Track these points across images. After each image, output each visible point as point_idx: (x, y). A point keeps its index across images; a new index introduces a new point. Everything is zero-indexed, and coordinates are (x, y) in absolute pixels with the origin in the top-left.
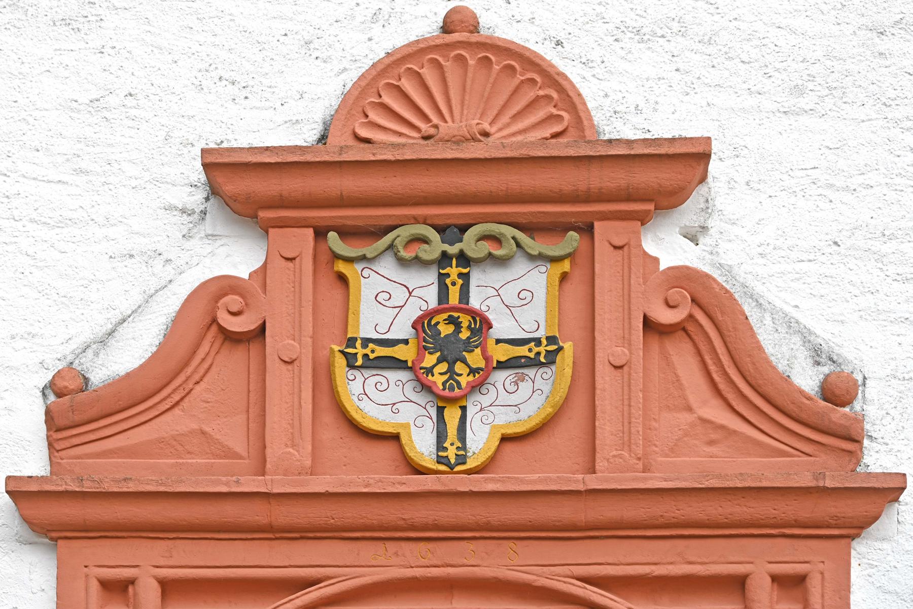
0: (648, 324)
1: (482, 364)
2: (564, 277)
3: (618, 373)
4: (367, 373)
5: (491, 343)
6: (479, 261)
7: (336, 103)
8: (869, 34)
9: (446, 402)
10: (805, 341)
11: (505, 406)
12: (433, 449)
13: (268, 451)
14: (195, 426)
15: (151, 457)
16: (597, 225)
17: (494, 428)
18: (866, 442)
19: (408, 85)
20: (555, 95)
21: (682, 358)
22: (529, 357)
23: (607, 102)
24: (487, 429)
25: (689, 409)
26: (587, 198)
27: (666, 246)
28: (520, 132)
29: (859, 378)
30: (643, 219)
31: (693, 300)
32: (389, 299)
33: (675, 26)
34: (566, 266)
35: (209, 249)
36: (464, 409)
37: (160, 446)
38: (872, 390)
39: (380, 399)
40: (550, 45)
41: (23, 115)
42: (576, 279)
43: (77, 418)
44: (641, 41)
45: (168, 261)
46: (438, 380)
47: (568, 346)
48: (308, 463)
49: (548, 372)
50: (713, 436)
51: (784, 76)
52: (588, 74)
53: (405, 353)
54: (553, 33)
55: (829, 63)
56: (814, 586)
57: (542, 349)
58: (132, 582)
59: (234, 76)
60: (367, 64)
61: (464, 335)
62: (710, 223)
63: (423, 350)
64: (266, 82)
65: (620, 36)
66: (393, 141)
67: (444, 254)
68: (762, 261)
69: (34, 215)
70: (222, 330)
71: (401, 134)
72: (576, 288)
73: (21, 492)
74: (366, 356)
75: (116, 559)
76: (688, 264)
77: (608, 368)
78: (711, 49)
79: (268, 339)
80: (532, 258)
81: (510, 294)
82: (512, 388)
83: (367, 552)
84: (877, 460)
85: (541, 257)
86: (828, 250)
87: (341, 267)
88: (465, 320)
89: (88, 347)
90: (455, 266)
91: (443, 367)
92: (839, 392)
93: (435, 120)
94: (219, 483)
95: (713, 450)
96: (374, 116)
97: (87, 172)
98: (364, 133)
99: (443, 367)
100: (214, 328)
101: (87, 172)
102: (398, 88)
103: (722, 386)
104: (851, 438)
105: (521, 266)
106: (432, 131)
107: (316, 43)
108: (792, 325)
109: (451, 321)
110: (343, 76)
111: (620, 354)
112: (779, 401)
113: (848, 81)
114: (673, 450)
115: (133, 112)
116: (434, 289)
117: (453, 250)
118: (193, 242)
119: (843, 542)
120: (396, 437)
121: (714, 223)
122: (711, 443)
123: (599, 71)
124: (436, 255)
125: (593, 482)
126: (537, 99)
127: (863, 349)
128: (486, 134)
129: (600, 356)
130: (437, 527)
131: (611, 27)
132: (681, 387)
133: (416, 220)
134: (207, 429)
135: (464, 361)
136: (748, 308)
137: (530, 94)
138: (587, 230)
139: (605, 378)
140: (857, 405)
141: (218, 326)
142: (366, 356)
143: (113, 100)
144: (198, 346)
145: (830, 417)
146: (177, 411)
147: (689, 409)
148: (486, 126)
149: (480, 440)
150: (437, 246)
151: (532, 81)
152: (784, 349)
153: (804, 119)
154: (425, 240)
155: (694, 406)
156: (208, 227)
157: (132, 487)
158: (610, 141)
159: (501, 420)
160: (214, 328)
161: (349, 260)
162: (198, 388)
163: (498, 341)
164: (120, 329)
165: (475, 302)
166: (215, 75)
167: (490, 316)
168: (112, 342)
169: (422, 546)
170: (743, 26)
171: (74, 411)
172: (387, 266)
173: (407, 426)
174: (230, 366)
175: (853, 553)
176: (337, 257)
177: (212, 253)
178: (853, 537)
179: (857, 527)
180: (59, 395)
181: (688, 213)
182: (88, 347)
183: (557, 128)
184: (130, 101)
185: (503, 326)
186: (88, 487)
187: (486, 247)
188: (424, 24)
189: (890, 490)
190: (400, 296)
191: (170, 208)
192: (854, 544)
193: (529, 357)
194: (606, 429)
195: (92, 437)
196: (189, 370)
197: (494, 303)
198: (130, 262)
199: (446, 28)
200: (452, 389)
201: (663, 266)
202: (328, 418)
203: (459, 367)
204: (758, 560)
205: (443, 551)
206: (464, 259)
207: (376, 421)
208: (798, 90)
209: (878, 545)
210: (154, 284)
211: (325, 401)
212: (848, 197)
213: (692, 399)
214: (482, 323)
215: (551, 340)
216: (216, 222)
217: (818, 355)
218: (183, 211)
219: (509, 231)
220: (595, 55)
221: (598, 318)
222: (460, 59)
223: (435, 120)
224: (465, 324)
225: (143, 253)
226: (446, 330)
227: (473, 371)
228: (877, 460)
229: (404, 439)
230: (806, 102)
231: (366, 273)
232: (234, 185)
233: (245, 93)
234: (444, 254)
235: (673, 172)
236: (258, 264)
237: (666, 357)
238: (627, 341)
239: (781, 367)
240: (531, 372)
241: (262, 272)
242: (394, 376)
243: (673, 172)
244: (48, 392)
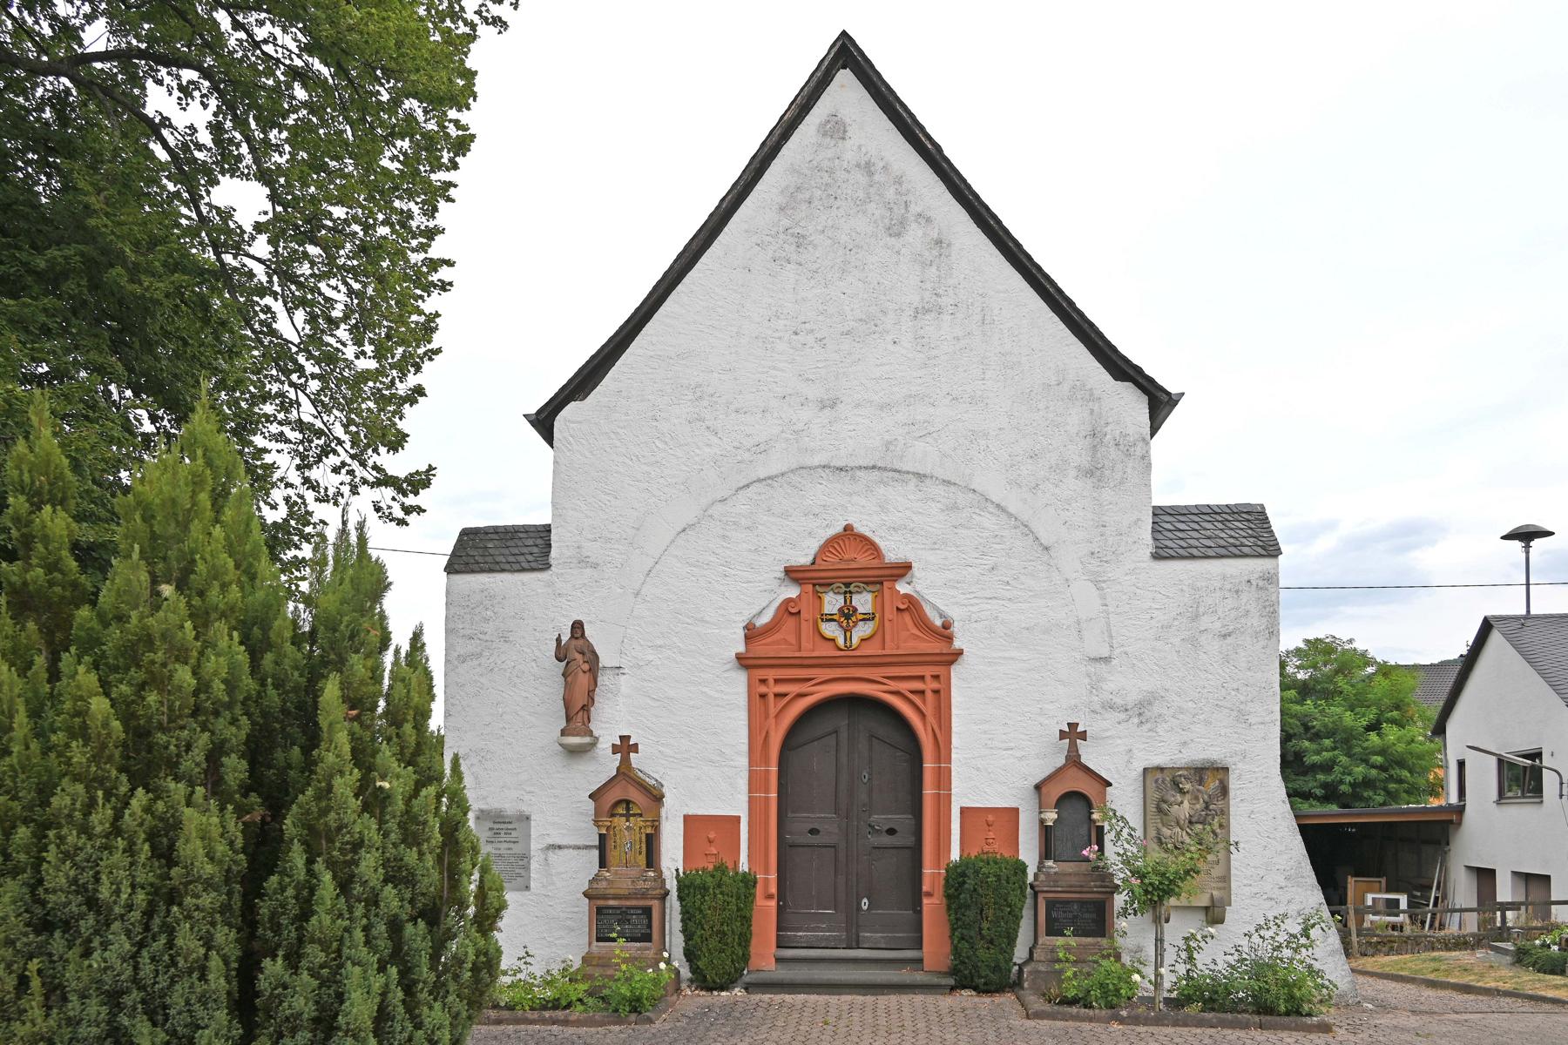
9: (847, 631)
11: (862, 631)
21: (907, 617)
22: (868, 618)
32: (832, 602)
37: (777, 643)
39: (830, 630)
73: (739, 657)
75: (762, 673)
84: (957, 644)
90: (848, 594)
92: (947, 626)
104: (950, 639)
108: (934, 607)
127: (954, 613)
139: (887, 624)
141: (788, 610)
145: (945, 633)
149: (855, 641)
171: (752, 634)
174: (791, 622)
179: (952, 663)
181: (907, 578)
185: (861, 610)
189: (960, 653)
193: (868, 618)
214: (855, 610)
217: (941, 616)
228: (957, 644)
235: (904, 569)
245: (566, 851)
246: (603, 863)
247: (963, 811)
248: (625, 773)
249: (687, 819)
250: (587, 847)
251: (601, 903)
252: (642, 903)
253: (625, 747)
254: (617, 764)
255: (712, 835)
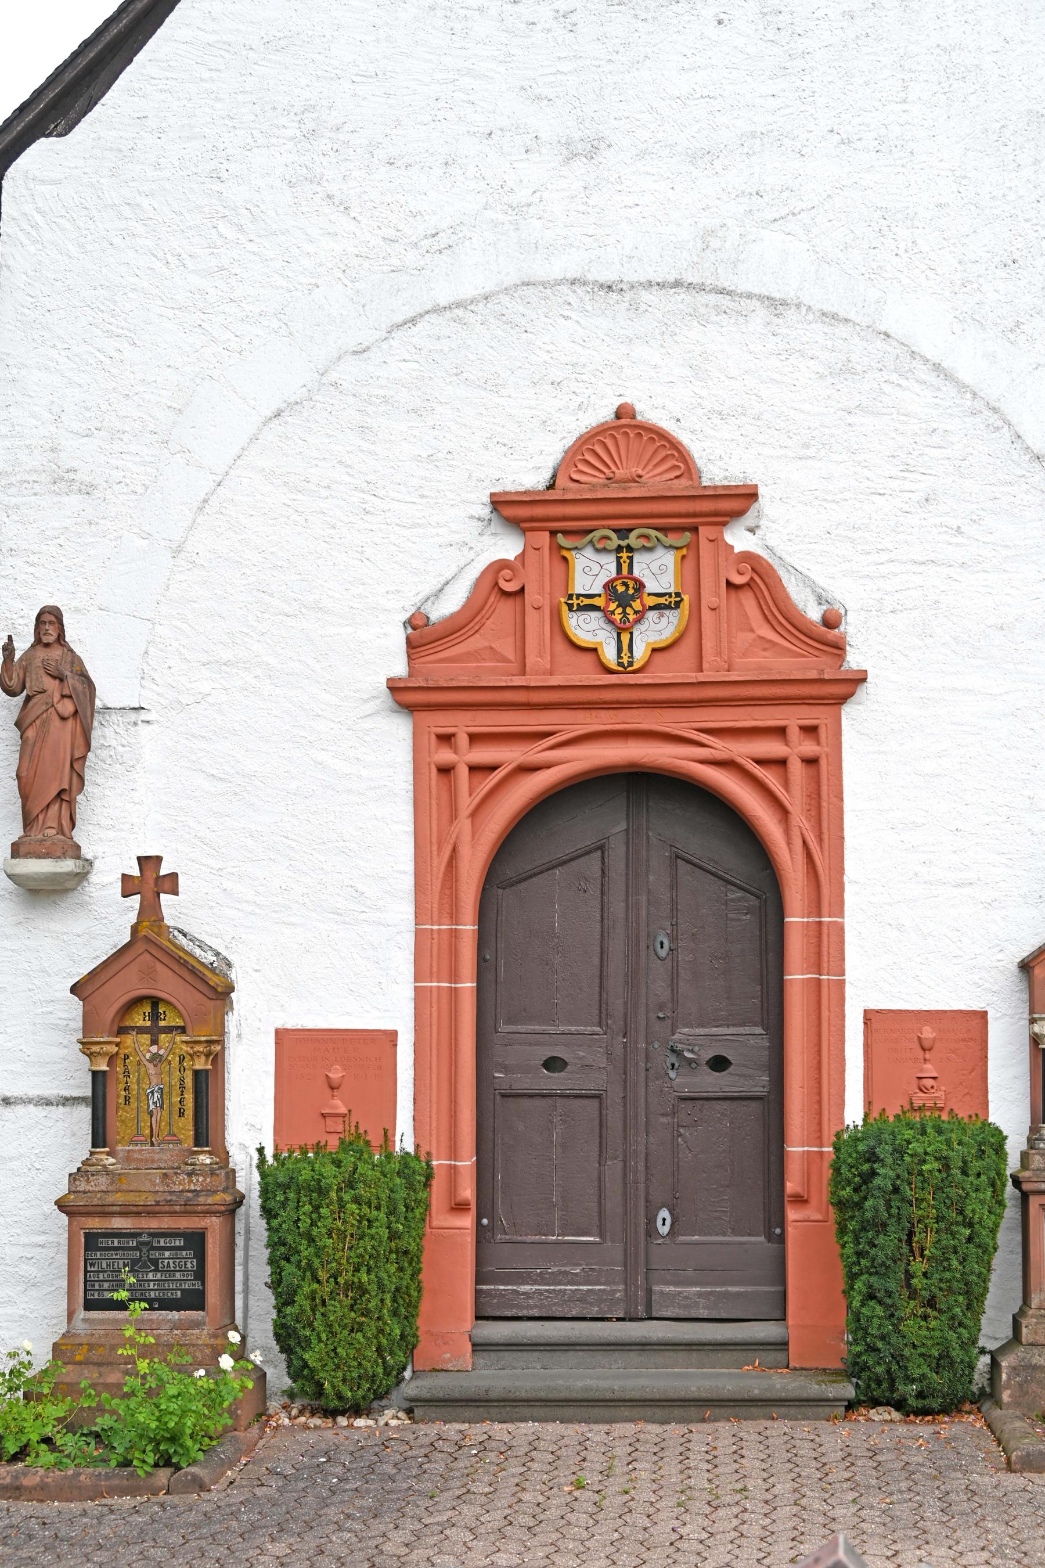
0: (729, 584)
1: (641, 609)
2: (683, 557)
3: (713, 612)
4: (579, 613)
5: (645, 596)
6: (637, 550)
7: (560, 456)
8: (843, 413)
9: (622, 630)
10: (813, 591)
11: (655, 630)
12: (616, 657)
13: (527, 660)
14: (487, 644)
15: (463, 662)
16: (701, 528)
17: (648, 644)
18: (848, 648)
19: (598, 449)
20: (676, 454)
21: (748, 601)
22: (667, 603)
23: (704, 453)
24: (644, 644)
25: (752, 630)
26: (694, 515)
27: (738, 539)
28: (658, 475)
29: (843, 612)
30: (724, 524)
31: (753, 569)
32: (591, 571)
33: (740, 410)
34: (684, 551)
35: (493, 541)
36: (631, 633)
38: (851, 618)
39: (587, 628)
40: (673, 421)
41: (392, 464)
42: (690, 559)
43: (424, 641)
44: (722, 419)
45: (471, 548)
46: (617, 617)
47: (686, 598)
48: (548, 666)
49: (676, 612)
50: (766, 646)
51: (798, 437)
52: (694, 438)
53: (599, 602)
54: (674, 414)
55: (822, 430)
56: (822, 731)
57: (672, 600)
58: (453, 735)
59: (505, 441)
60: (576, 435)
61: (631, 592)
62: (761, 523)
63: (609, 601)
64: (522, 445)
65: (711, 416)
66: (591, 478)
67: (619, 546)
68: (789, 543)
69: (398, 522)
70: (500, 589)
71: (595, 476)
72: (690, 563)
73: (395, 687)
74: (578, 604)
75: (444, 721)
76: (751, 550)
77: (708, 610)
78: (759, 423)
79: (526, 596)
80: (666, 547)
81: (654, 567)
82: (657, 621)
83: (581, 716)
84: (854, 660)
85: (671, 547)
86: (824, 537)
87: (565, 553)
88: (631, 584)
89: (428, 598)
90: (625, 553)
91: (620, 610)
93: (614, 468)
94: (502, 680)
95: (765, 654)
96: (582, 467)
97: (427, 497)
98: (575, 477)
99: (620, 610)
100: (496, 588)
101: (427, 497)
102: (593, 451)
103: (770, 617)
104: (838, 648)
105: (660, 552)
106: (611, 475)
107: (548, 423)
108: (807, 581)
109: (624, 584)
110: (564, 441)
111: (714, 601)
112: (800, 627)
113: (833, 440)
114: (744, 655)
115: (451, 462)
116: (614, 564)
117: (624, 543)
118: (484, 537)
119: (837, 707)
120: (595, 650)
121: (763, 522)
122: (765, 650)
123: (700, 436)
124: (615, 546)
125: (701, 677)
126: (667, 456)
128: (640, 477)
129: (703, 602)
130: (618, 702)
131: (705, 411)
132: (748, 618)
133: (604, 527)
134: (493, 646)
135: (631, 606)
136: (781, 572)
137: (663, 453)
138: (694, 530)
139: (706, 615)
140: (842, 628)
141: (498, 587)
142: (578, 604)
143: (440, 456)
144: (488, 598)
145: (826, 637)
146: (477, 635)
147: (752, 630)
148: (640, 472)
149: (640, 652)
150: (615, 541)
151: (664, 446)
152: (802, 596)
153: (810, 462)
154: (608, 538)
155: (755, 628)
156: (493, 528)
157: (454, 684)
158: (705, 487)
159: (651, 640)
160: (496, 588)
161: (569, 549)
162: (488, 622)
163: (649, 594)
164: (446, 588)
165: (636, 573)
166: (495, 440)
167: (644, 580)
168: (441, 596)
169: (611, 712)
170: (776, 409)
171: (422, 637)
172: (589, 552)
173: (601, 643)
174: (506, 609)
175: (843, 712)
176: (561, 548)
177: (495, 544)
178: (842, 704)
180: (414, 628)
181: (749, 519)
182: (428, 598)
183: (678, 473)
184: (449, 456)
185: (651, 586)
186: (431, 684)
187: (642, 542)
188: (604, 413)
189: (859, 679)
190: (596, 568)
191: (472, 517)
192: (843, 707)
193: (667, 603)
194: (708, 645)
195: (431, 651)
196: (484, 612)
197: (646, 572)
198: (450, 548)
199: (618, 415)
200: (625, 623)
201: (736, 551)
202: (559, 639)
203: (629, 610)
204: (792, 718)
205: (622, 715)
206: (630, 549)
207: (585, 641)
208: (806, 446)
209: (856, 707)
210: (463, 563)
211: (557, 629)
212: (834, 506)
213: (754, 625)
214: (640, 586)
215: (678, 594)
216: (496, 526)
217: (820, 600)
218: (479, 519)
219: (653, 533)
220: (697, 427)
221: (702, 569)
222: (626, 433)
223: (614, 468)
224: (631, 586)
225: (458, 543)
226: (621, 589)
227: (636, 612)
228: (854, 660)
229: (600, 652)
230: (811, 452)
231: (578, 556)
232: (510, 511)
233: (511, 451)
234: (619, 546)
235: (742, 499)
236: (519, 551)
237: (739, 601)
238: (717, 594)
239: (801, 606)
240: (667, 612)
241: (522, 557)
242: (594, 615)
243: (742, 499)
244: (407, 625)
245: (20, 1110)
246: (99, 1138)
247: (289, 1043)
248: (150, 938)
249: (282, 1036)
250: (66, 1101)
251: (95, 1224)
252: (184, 1223)
253: (150, 881)
254: (133, 918)
255: (335, 1075)
